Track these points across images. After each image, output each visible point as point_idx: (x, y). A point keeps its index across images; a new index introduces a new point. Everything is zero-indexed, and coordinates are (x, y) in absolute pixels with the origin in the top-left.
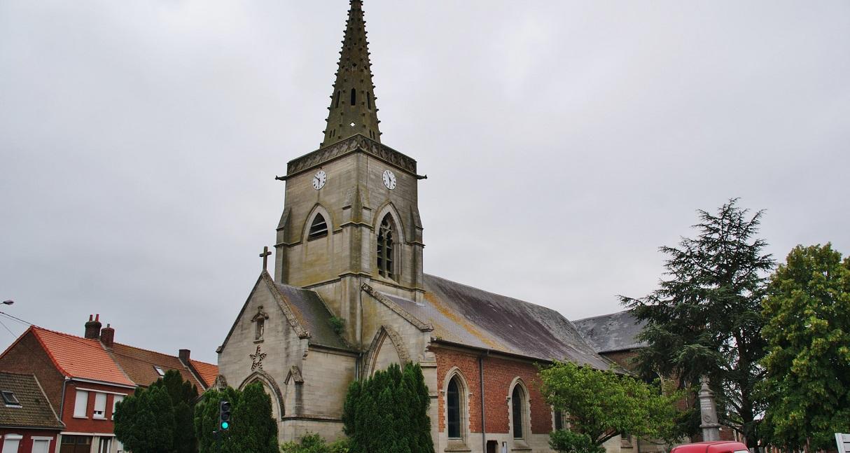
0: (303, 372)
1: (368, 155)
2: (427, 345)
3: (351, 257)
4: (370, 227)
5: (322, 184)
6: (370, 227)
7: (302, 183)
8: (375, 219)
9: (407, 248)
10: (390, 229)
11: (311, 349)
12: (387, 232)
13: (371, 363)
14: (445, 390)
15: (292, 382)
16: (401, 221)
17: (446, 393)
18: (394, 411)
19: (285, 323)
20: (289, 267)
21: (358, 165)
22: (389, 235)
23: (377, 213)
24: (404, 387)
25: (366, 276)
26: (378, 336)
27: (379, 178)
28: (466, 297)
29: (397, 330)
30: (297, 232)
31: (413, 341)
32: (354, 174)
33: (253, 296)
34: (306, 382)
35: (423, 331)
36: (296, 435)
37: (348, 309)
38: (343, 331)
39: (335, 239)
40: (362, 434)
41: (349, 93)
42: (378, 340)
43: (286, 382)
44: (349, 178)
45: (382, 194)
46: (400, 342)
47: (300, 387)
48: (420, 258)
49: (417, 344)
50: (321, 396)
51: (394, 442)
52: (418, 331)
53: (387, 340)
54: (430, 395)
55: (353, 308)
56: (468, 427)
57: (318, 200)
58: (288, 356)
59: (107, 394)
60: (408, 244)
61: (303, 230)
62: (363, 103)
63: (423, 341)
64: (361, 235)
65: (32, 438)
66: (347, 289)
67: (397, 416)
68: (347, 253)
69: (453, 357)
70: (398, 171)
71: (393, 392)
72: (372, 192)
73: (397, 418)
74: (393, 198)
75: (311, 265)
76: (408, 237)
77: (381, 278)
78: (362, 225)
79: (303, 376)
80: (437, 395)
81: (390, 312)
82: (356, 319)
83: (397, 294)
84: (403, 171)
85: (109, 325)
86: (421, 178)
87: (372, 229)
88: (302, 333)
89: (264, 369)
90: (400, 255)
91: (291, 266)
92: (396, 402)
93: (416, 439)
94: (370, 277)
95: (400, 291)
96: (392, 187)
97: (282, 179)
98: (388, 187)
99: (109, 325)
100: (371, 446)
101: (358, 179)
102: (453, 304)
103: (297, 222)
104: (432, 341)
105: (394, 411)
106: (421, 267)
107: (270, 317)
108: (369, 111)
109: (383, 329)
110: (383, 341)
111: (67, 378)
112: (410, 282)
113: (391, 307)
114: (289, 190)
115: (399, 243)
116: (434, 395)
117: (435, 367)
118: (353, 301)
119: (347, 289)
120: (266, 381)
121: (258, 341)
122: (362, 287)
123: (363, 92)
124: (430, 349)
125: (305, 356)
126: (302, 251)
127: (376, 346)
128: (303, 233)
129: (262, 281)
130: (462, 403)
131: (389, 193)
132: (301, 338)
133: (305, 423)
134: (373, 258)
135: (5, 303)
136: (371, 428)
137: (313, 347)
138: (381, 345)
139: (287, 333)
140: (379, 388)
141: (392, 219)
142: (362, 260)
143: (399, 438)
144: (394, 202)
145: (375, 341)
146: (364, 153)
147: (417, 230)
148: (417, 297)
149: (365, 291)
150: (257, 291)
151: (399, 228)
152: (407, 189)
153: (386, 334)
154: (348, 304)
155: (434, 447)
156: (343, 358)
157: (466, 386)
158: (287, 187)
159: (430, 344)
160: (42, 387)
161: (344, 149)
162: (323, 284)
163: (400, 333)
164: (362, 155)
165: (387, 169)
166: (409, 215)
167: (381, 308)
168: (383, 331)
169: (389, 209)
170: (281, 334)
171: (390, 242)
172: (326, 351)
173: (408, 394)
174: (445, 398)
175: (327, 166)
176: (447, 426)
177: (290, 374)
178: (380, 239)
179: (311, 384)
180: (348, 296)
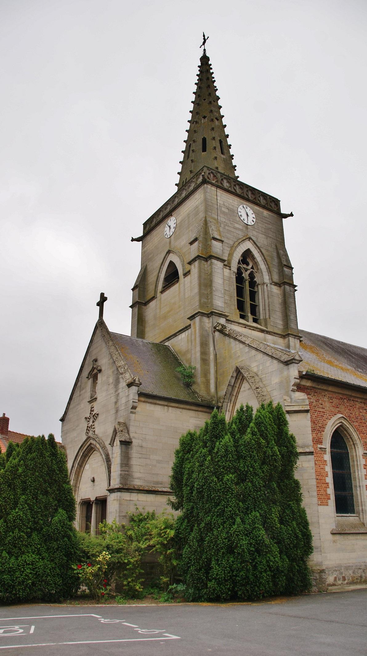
0: (132, 429)
1: (217, 187)
2: (293, 381)
3: (201, 294)
4: (223, 261)
5: (172, 230)
6: (223, 261)
7: (155, 237)
8: (231, 255)
9: (275, 290)
10: (252, 268)
11: (143, 399)
12: (248, 272)
14: (327, 444)
15: (117, 443)
16: (265, 260)
17: (328, 450)
18: (236, 470)
19: (116, 372)
20: (145, 327)
21: (205, 196)
22: (252, 276)
23: (233, 248)
24: (253, 434)
25: (220, 315)
26: (233, 381)
27: (233, 213)
28: (357, 355)
29: (255, 370)
30: (151, 288)
31: (276, 380)
32: (202, 208)
33: (91, 350)
35: (287, 363)
36: (120, 511)
37: (198, 354)
38: (194, 383)
39: (186, 283)
40: (193, 508)
41: (200, 142)
42: (233, 387)
43: (112, 444)
44: (197, 214)
45: (239, 229)
46: (261, 384)
47: (127, 449)
48: (291, 300)
49: (281, 383)
50: (159, 462)
51: (238, 520)
52: (281, 365)
53: (245, 385)
54: (299, 450)
55: (204, 353)
57: (170, 247)
58: (117, 411)
60: (276, 284)
62: (215, 148)
63: (288, 377)
64: (211, 268)
66: (197, 331)
67: (242, 478)
68: (196, 290)
69: (335, 401)
70: (256, 208)
71: (236, 441)
72: (225, 225)
73: (243, 481)
74: (252, 234)
75: (165, 317)
76: (276, 278)
77: (242, 321)
78: (211, 257)
79: (132, 435)
80: (311, 449)
81: (247, 349)
82: (209, 365)
84: (264, 207)
85: (4, 414)
86: (286, 216)
87: (228, 265)
88: (130, 380)
89: (96, 433)
90: (266, 296)
91: (147, 325)
92: (240, 457)
93: (275, 517)
94: (225, 316)
96: (250, 223)
97: (138, 240)
98: (246, 222)
99: (4, 414)
100: (203, 525)
101: (206, 211)
102: (341, 358)
103: (151, 278)
104: (302, 377)
105: (236, 470)
106: (293, 310)
107: (103, 369)
108: (222, 156)
109: (238, 371)
110: (239, 388)
112: (281, 327)
113: (247, 342)
115: (264, 284)
116: (308, 450)
117: (307, 411)
118: (204, 345)
119: (197, 331)
120: (98, 446)
121: (93, 400)
122: (215, 328)
123: (214, 138)
124: (299, 388)
125: (134, 408)
126: (156, 305)
127: (231, 394)
128: (156, 286)
129: (98, 332)
130: (354, 466)
131: (247, 228)
132: (129, 385)
133: (134, 497)
134: (231, 297)
135: (205, 60)
136: (203, 497)
137: (144, 396)
138: (238, 393)
139: (117, 382)
140: (216, 438)
141: (253, 258)
142: (214, 297)
143: (247, 511)
145: (230, 388)
146: (213, 185)
148: (292, 344)
149: (218, 330)
150: (93, 343)
151: (262, 266)
152: (270, 226)
153: (243, 378)
154: (198, 348)
155: (311, 528)
156: (192, 413)
157: (358, 442)
158: (143, 247)
159: (298, 381)
161: (193, 186)
162: (175, 335)
163: (259, 373)
164: (209, 186)
165: (242, 204)
166: (275, 254)
167: (236, 347)
168: (239, 375)
169: (248, 245)
170: (112, 386)
171: (253, 284)
172: (166, 403)
173: (259, 444)
174: (327, 457)
175: (177, 211)
176: (333, 497)
177: (115, 432)
178: (239, 279)
179: (144, 444)
180: (198, 340)
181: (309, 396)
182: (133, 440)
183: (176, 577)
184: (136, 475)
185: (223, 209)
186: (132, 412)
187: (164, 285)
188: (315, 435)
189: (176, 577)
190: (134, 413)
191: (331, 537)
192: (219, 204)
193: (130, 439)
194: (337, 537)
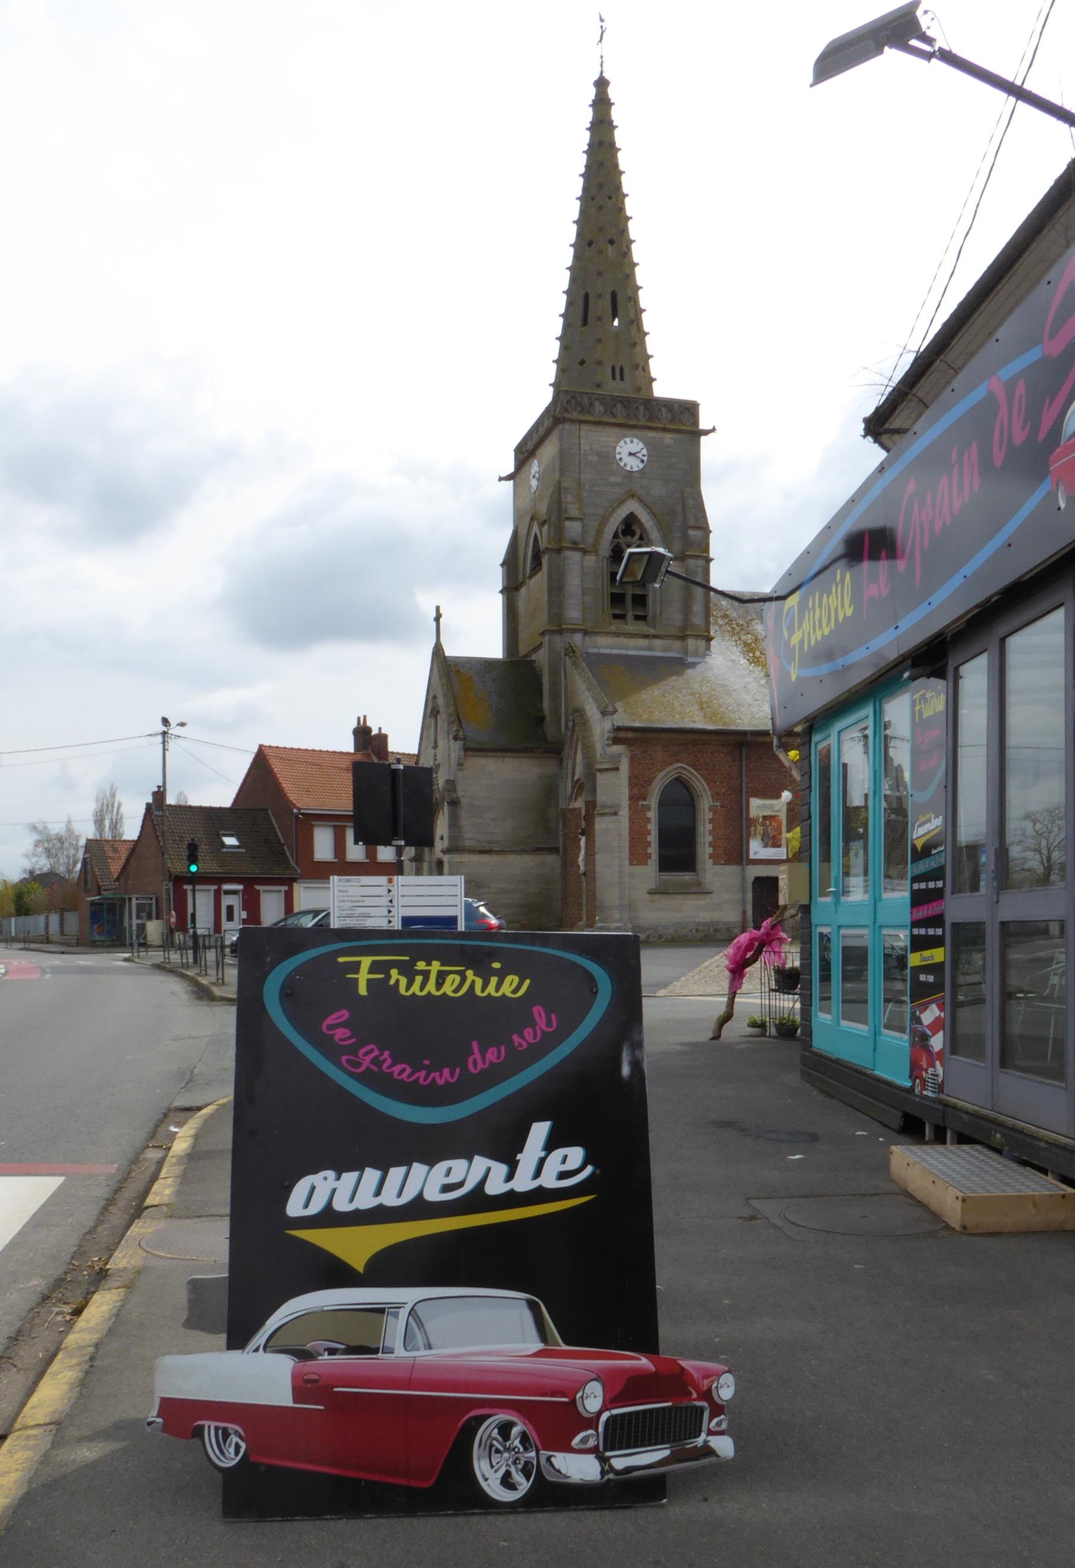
0: (459, 787)
11: (470, 753)
13: (570, 766)
34: (464, 801)
56: (707, 856)
59: (335, 826)
61: (694, 527)
65: (257, 887)
83: (650, 649)
85: (380, 729)
95: (658, 642)
99: (380, 729)
111: (295, 811)
114: (907, 391)
135: (602, 84)
144: (641, 492)
146: (573, 421)
147: (692, 533)
158: (515, 486)
160: (277, 824)
172: (500, 754)
181: (632, 748)
182: (462, 800)
183: (1053, 1017)
184: (467, 835)
185: (590, 458)
186: (459, 770)
187: (534, 566)
188: (635, 791)
189: (1053, 1017)
190: (461, 770)
191: (648, 897)
192: (582, 452)
193: (458, 798)
194: (657, 897)
